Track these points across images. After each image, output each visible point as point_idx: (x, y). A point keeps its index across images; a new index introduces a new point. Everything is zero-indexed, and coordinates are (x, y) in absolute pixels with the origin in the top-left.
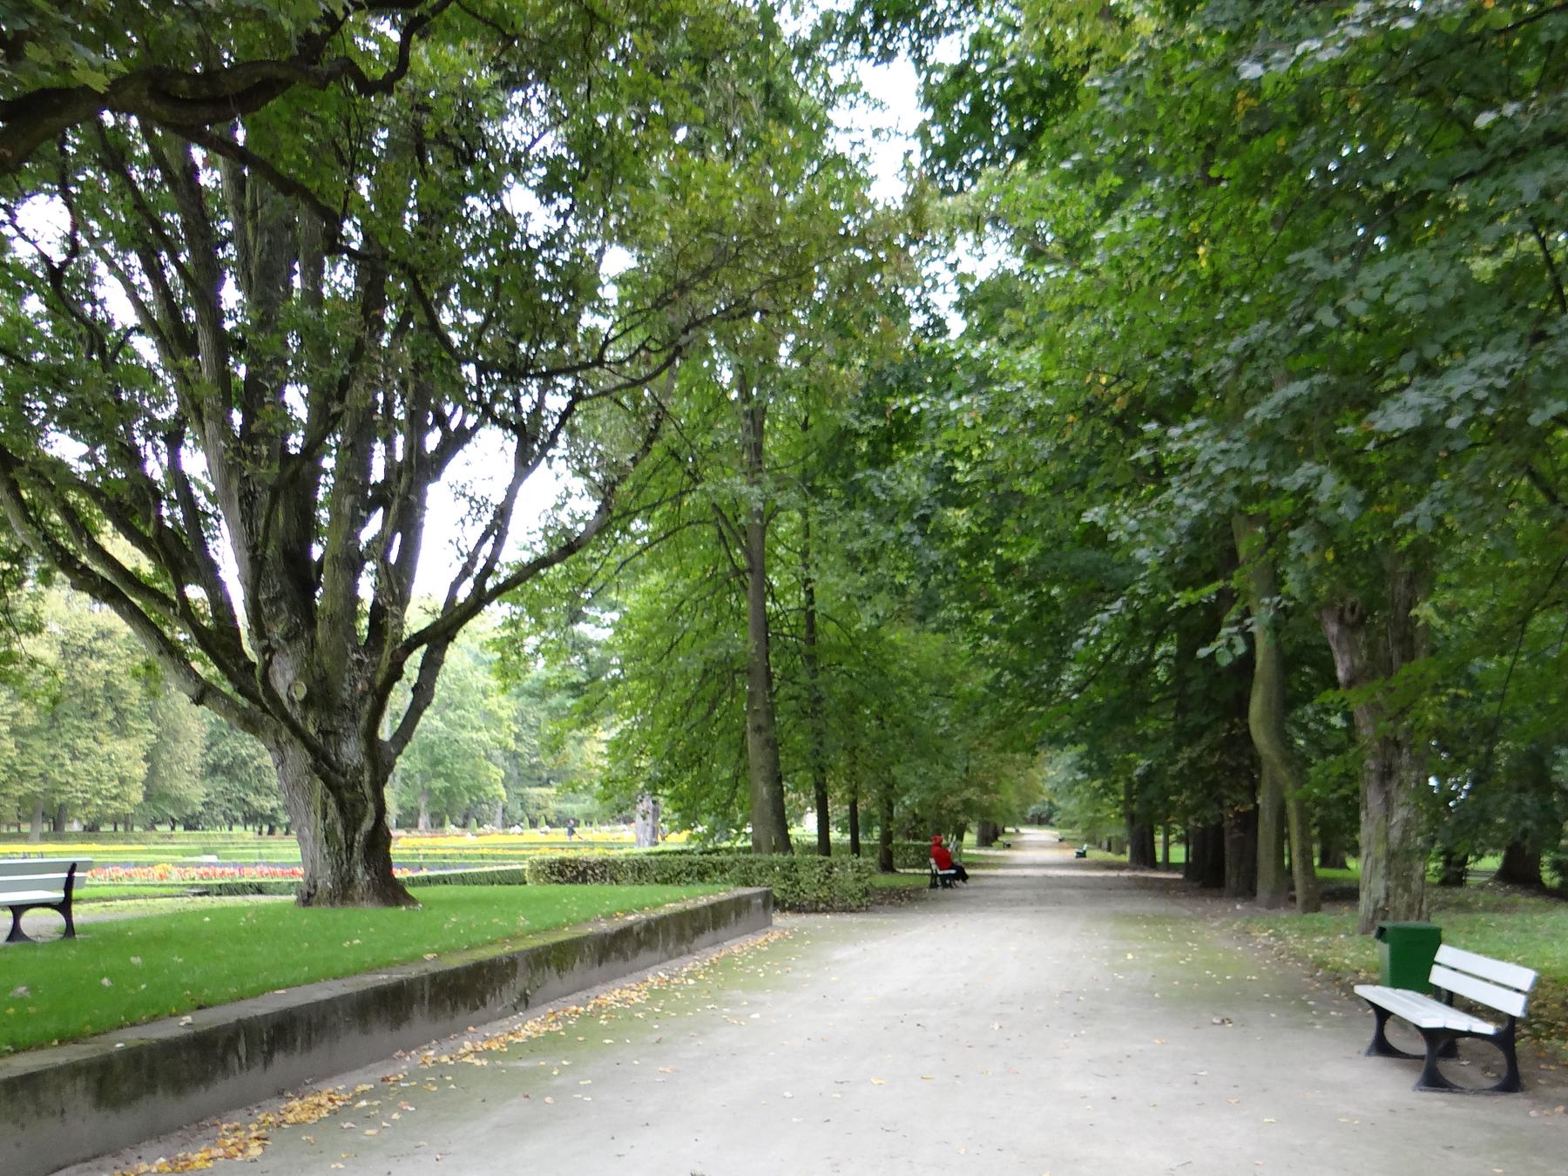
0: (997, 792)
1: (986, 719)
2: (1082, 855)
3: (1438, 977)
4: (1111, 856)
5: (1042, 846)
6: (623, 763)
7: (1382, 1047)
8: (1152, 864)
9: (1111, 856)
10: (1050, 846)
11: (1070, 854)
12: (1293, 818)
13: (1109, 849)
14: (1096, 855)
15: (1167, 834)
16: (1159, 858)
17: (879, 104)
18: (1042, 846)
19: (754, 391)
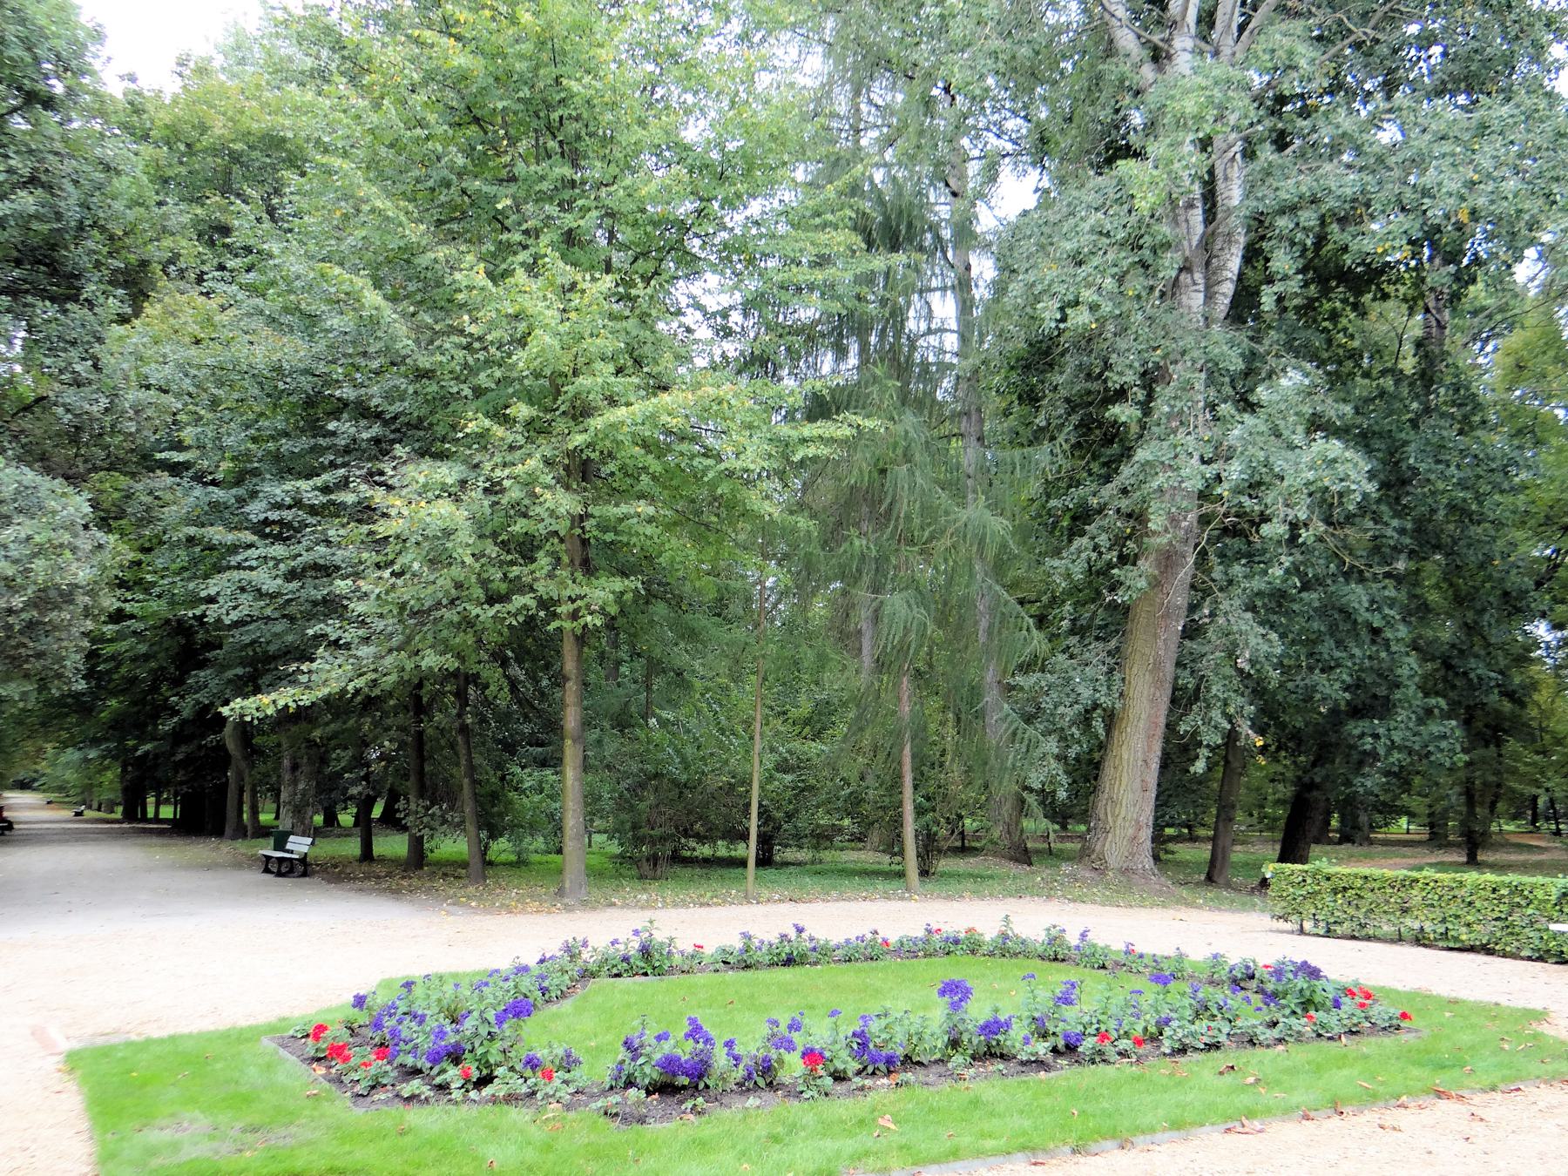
0: (924, 873)
1: (89, 625)
2: (77, 814)
3: (777, 858)
4: (102, 815)
5: (31, 807)
6: (1473, 557)
7: (267, 871)
8: (145, 819)
9: (102, 815)
10: (41, 808)
11: (69, 814)
12: (247, 788)
13: (99, 809)
14: (89, 814)
15: (158, 797)
16: (151, 813)
17: (568, 1063)
18: (31, 807)
19: (1518, 393)
